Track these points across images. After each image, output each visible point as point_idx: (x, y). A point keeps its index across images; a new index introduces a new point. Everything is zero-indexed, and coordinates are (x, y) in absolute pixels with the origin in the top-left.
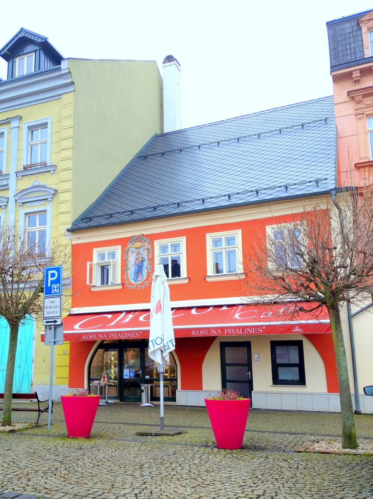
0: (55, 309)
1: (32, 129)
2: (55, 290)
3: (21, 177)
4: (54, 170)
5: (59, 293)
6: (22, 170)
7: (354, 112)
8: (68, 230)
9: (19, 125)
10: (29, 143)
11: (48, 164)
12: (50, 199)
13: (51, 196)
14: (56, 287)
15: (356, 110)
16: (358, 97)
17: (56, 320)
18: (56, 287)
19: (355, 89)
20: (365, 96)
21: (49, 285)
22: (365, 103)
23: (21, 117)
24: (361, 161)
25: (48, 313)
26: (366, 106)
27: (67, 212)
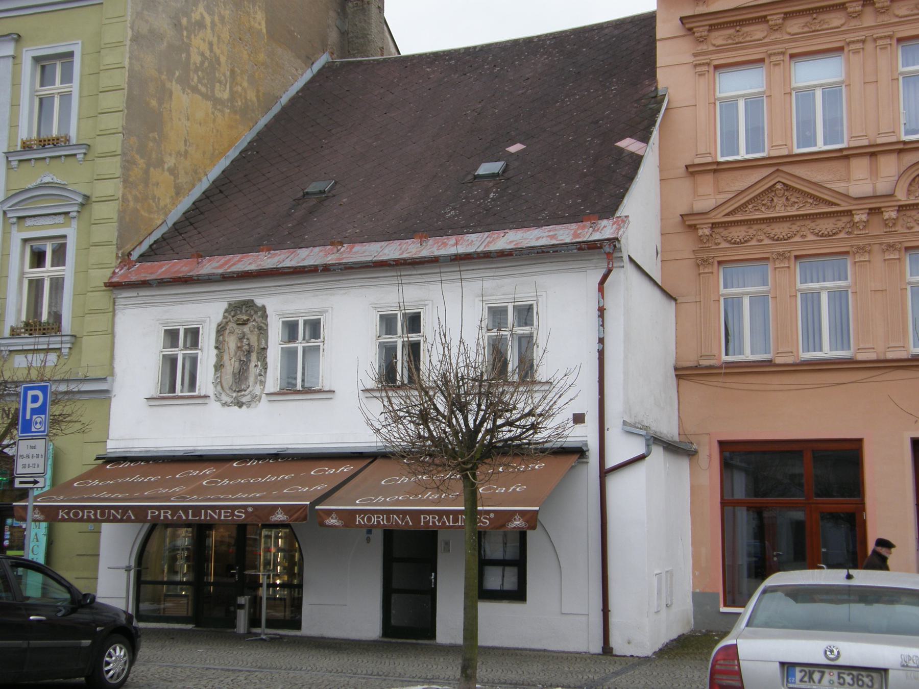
0: (35, 460)
1: (43, 64)
2: (38, 426)
3: (17, 163)
4: (85, 154)
5: (44, 431)
6: (19, 148)
7: (691, 59)
8: (106, 285)
9: (16, 49)
10: (37, 91)
11: (74, 141)
12: (74, 214)
13: (76, 208)
14: (39, 420)
15: (695, 55)
16: (701, 29)
17: (37, 479)
18: (39, 420)
19: (697, 13)
20: (712, 28)
21: (28, 417)
22: (714, 42)
23: (19, 36)
24: (697, 161)
25: (24, 466)
26: (714, 48)
27: (107, 244)
